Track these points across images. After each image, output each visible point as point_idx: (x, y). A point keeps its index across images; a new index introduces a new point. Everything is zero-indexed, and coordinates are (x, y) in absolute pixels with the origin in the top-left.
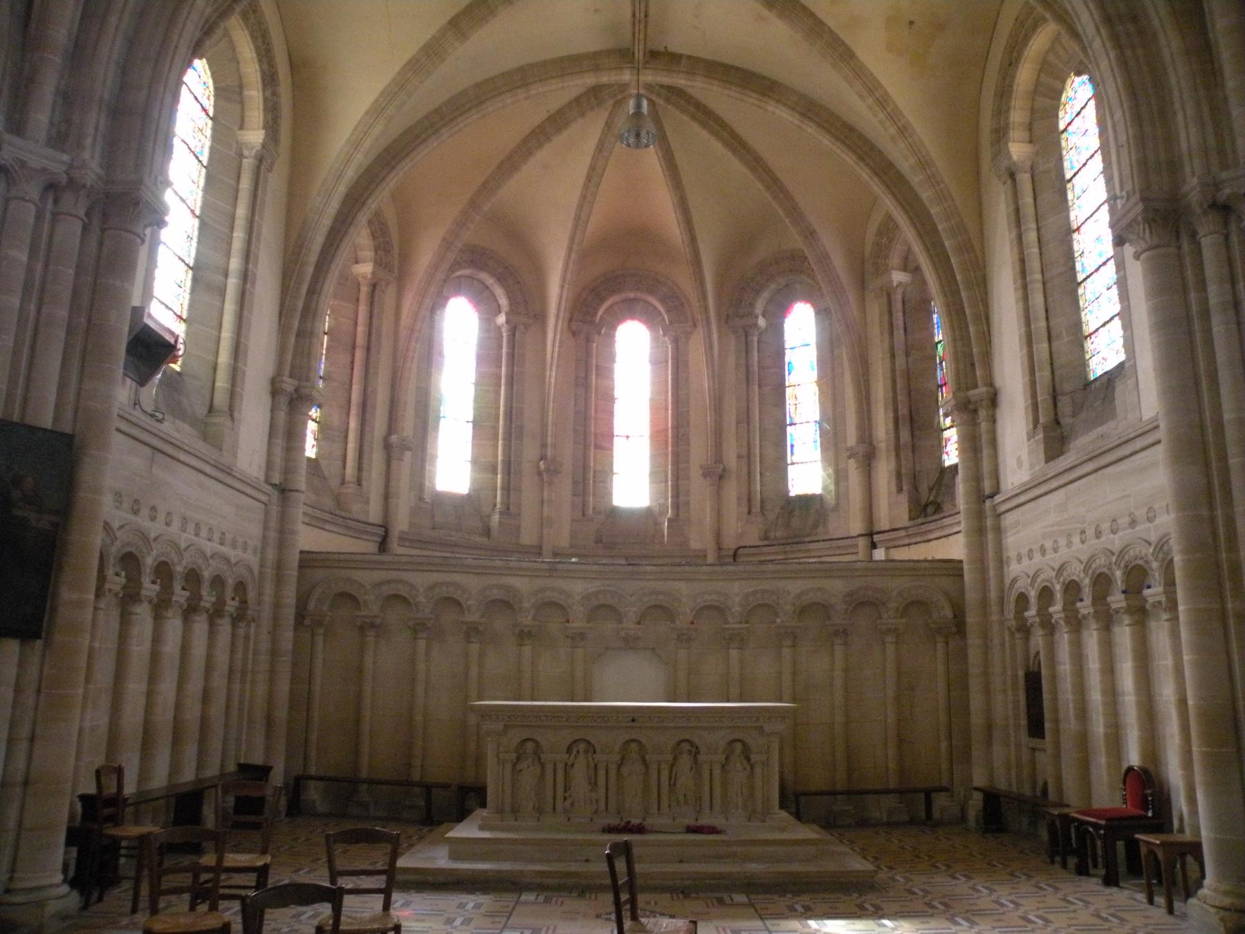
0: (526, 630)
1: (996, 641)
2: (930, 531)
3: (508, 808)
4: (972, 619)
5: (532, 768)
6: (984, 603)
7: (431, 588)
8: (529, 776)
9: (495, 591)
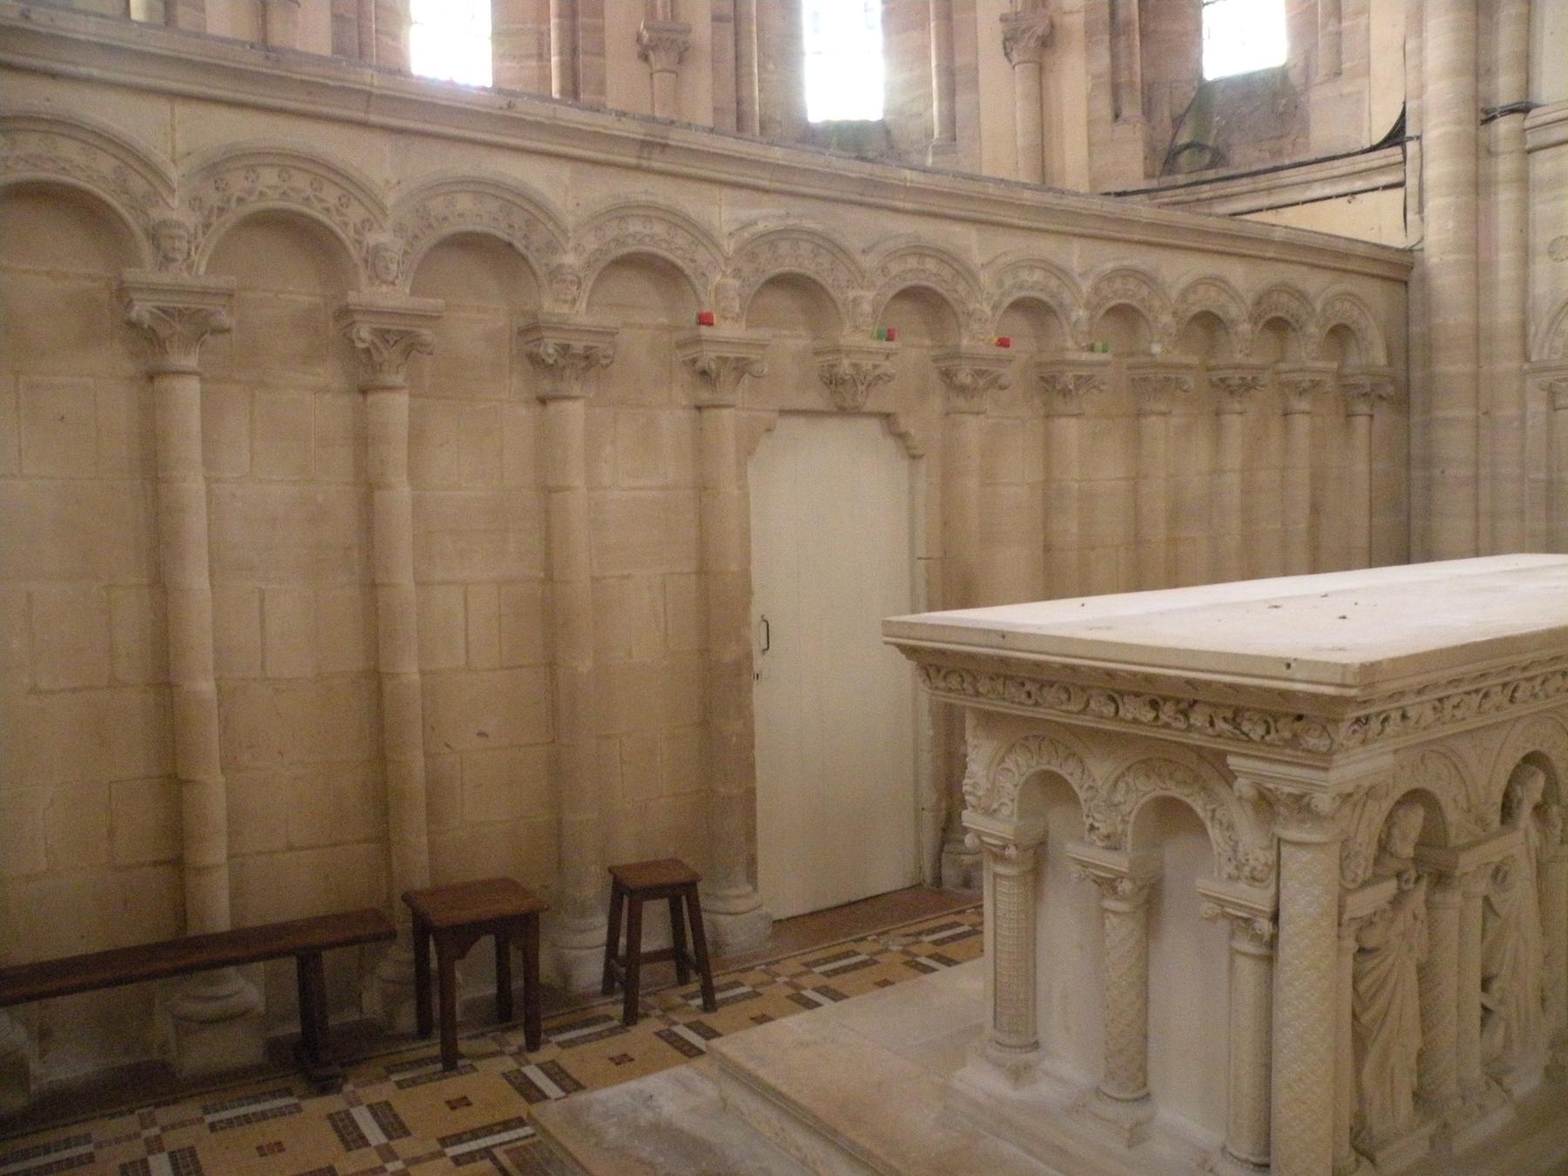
0: (579, 346)
2: (1308, 183)
4: (1452, 367)
6: (1480, 337)
7: (213, 169)
9: (464, 203)
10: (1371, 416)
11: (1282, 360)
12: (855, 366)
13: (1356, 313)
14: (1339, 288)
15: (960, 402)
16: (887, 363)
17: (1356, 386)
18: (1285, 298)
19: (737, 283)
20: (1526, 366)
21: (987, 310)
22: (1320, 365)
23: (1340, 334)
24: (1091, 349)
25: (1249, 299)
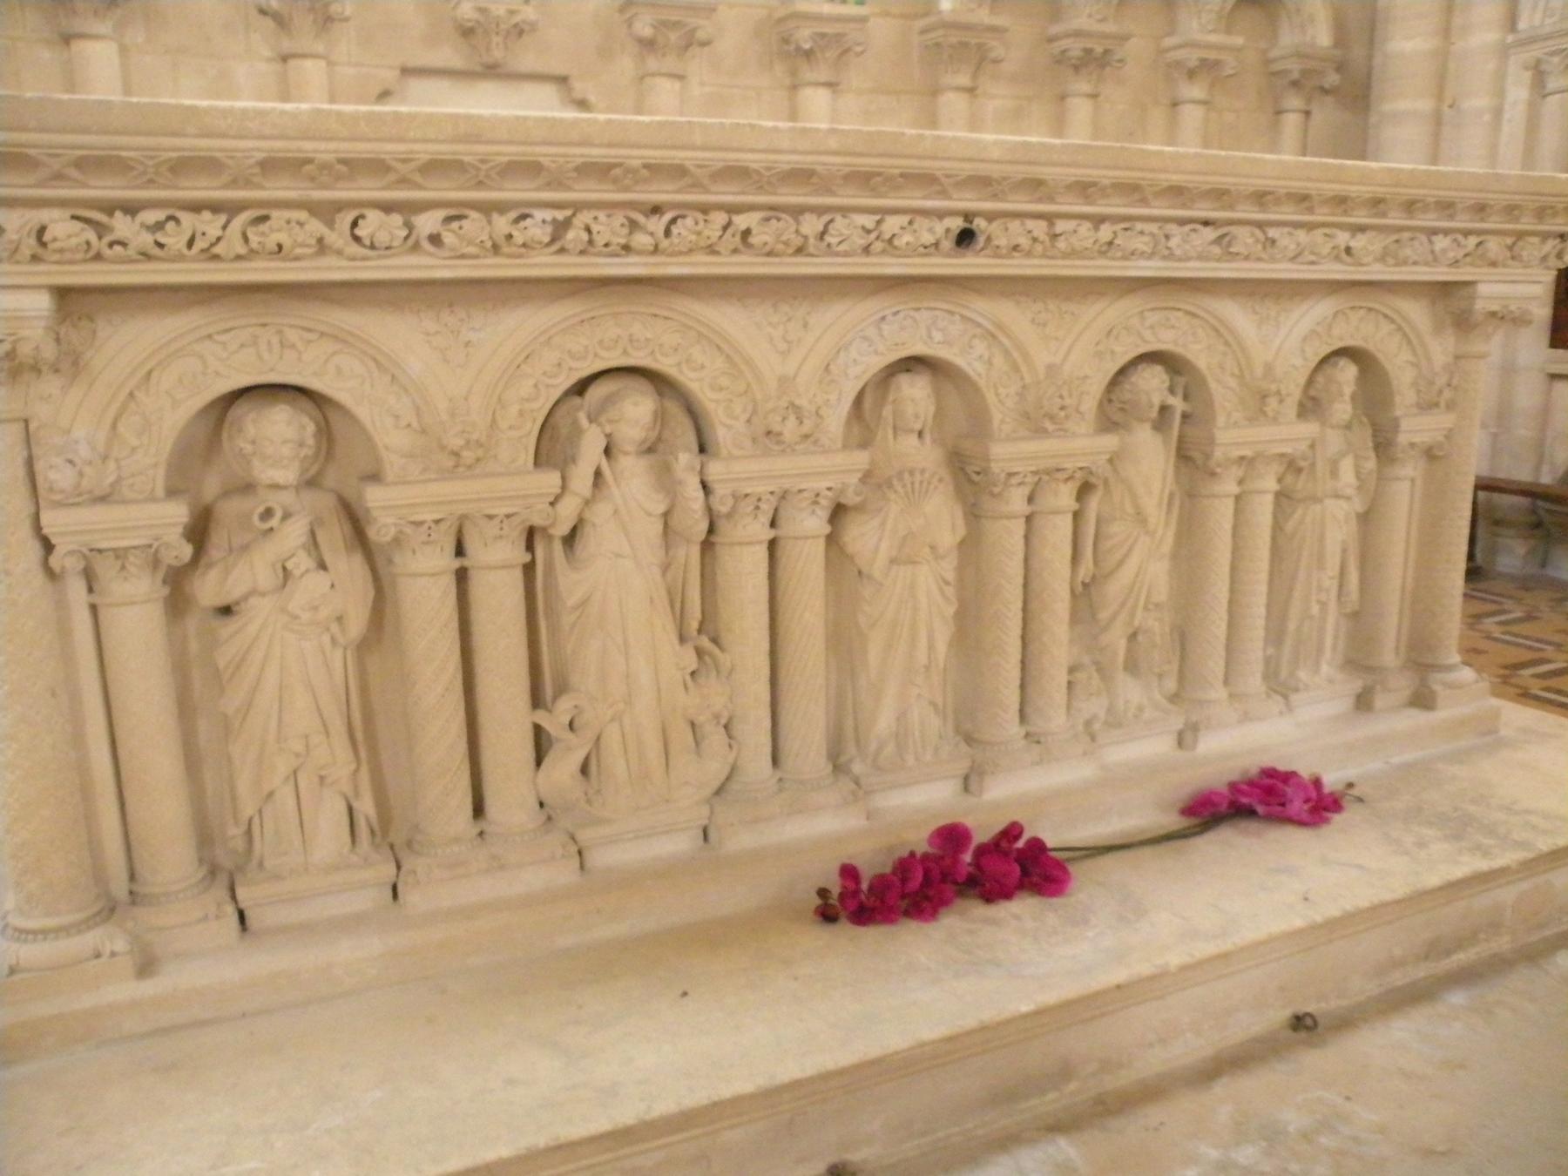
1: (1479, 102)
5: (316, 583)
8: (291, 623)
10: (1307, 113)
11: (1171, 34)
15: (652, 63)
20: (1510, 38)
22: (1213, 38)
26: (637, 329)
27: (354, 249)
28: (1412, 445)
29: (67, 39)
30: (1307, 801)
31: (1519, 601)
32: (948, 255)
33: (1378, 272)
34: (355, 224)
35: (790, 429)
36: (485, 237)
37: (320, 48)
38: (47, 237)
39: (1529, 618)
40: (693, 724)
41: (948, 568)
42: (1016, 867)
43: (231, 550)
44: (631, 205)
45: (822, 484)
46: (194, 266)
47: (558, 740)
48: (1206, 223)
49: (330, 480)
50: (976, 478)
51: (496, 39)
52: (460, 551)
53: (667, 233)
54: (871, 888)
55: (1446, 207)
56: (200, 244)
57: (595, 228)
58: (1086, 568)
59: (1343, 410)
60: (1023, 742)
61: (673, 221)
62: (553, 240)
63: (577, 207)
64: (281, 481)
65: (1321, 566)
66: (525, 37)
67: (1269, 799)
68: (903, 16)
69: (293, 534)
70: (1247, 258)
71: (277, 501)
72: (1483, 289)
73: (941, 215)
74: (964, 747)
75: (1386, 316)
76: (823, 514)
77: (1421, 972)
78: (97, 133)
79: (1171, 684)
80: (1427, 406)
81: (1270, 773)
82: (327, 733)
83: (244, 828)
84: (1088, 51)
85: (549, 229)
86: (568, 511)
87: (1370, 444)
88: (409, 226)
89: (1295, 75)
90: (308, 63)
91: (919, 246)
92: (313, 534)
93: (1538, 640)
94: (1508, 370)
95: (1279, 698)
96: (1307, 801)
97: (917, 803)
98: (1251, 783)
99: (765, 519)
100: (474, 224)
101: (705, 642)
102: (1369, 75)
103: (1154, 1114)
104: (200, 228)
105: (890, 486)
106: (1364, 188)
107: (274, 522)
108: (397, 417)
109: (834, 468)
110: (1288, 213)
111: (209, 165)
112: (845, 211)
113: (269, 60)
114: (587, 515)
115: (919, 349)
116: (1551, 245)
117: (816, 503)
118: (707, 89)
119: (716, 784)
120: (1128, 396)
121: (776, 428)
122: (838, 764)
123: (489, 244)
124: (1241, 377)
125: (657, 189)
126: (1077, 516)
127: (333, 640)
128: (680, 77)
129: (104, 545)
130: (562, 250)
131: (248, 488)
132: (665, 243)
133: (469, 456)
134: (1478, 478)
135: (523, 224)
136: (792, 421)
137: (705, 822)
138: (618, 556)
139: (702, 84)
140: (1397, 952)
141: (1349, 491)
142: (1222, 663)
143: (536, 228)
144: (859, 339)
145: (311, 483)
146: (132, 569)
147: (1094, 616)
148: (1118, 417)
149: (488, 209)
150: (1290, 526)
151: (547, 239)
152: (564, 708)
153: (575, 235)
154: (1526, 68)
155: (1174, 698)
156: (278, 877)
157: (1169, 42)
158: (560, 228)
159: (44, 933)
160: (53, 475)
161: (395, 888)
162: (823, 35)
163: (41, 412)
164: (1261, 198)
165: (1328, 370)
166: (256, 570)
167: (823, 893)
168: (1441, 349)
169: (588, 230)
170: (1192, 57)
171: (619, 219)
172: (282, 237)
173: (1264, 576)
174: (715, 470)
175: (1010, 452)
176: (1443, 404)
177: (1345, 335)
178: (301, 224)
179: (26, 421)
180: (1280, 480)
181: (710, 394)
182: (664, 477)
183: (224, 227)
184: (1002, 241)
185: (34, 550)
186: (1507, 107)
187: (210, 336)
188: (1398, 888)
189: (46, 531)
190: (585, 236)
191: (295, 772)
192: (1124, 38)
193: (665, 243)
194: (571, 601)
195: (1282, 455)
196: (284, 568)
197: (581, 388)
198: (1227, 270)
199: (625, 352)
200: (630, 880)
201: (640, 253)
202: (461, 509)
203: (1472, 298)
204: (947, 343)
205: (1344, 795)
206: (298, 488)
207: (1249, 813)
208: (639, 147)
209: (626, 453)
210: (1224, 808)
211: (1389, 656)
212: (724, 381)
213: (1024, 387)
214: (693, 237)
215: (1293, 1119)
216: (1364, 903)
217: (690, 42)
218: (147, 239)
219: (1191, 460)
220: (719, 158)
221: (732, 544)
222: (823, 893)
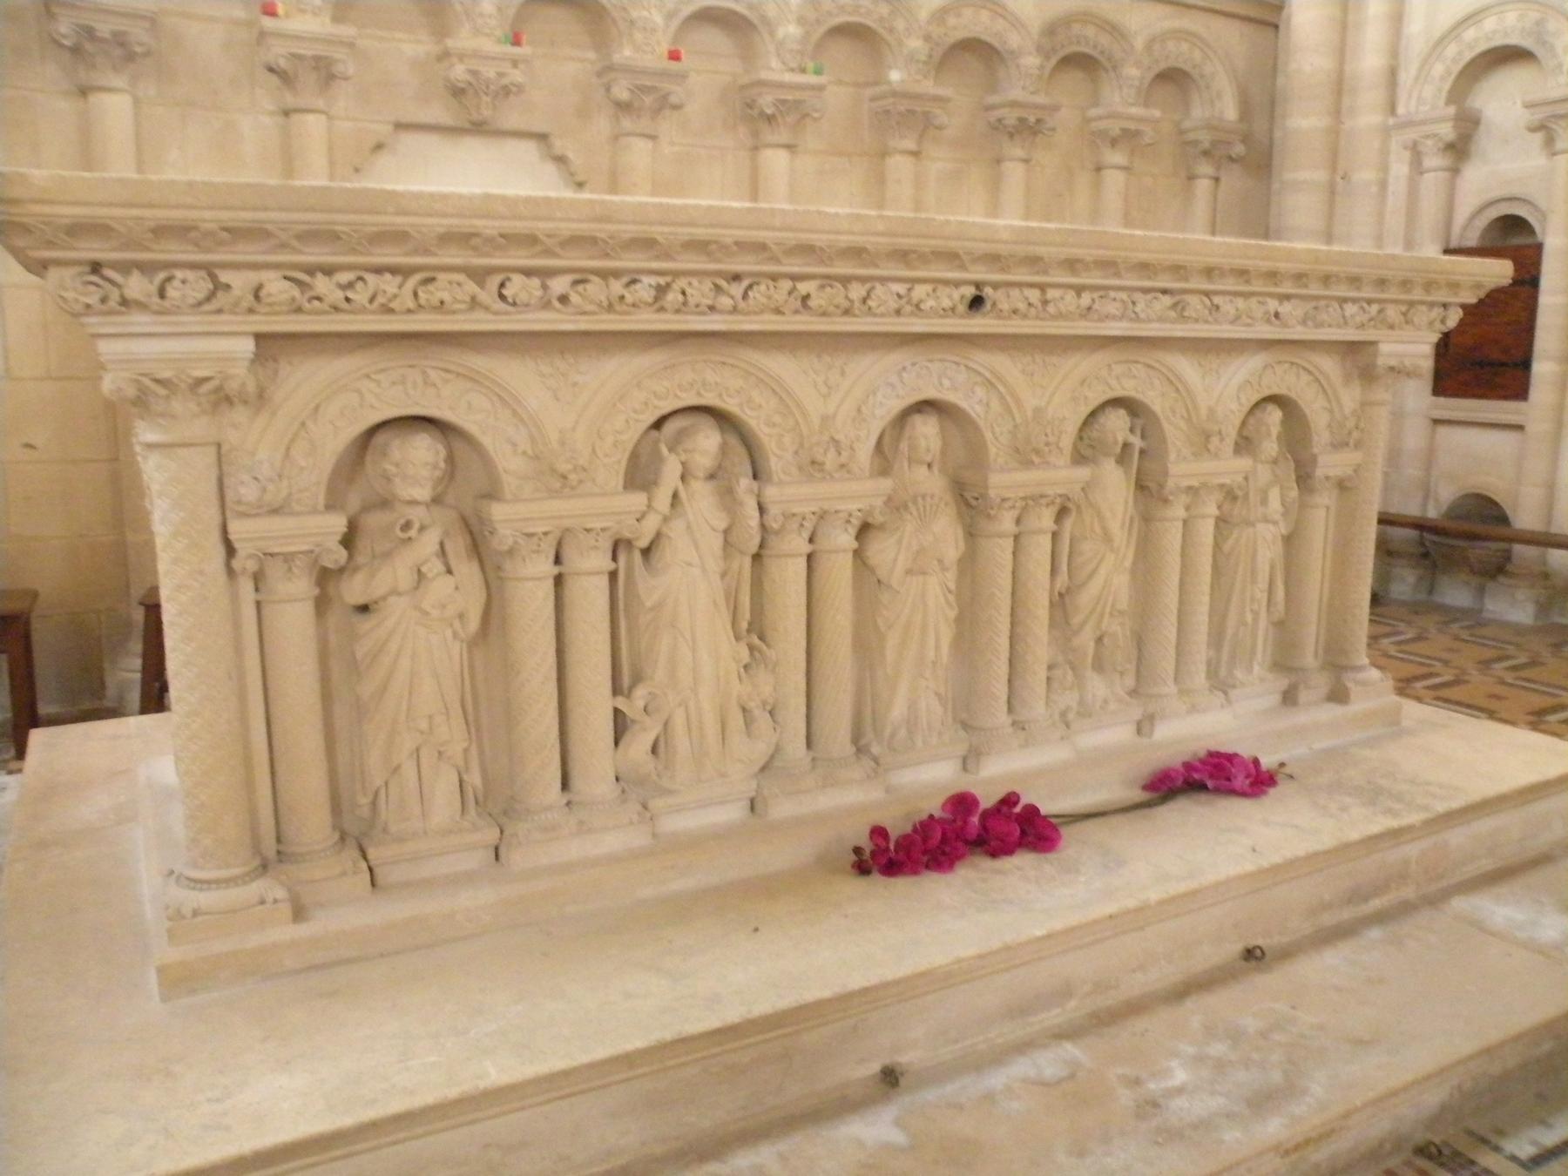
1: (1366, 175)
3: (313, 825)
4: (1304, 121)
5: (441, 587)
6: (1340, 86)
8: (422, 619)
10: (1217, 179)
11: (1096, 104)
12: (474, 73)
13: (1197, 55)
14: (1168, 24)
15: (627, 124)
16: (516, 72)
17: (1195, 143)
18: (1090, 31)
19: (1230, 112)
20: (1391, 121)
21: (658, 19)
22: (1134, 110)
23: (1173, 79)
24: (803, 71)
25: (1035, 27)
26: (710, 376)
27: (501, 306)
28: (1327, 478)
29: (84, 92)
30: (1247, 777)
31: (1409, 623)
32: (962, 317)
33: (1298, 333)
34: (502, 285)
35: (830, 460)
36: (603, 298)
37: (320, 103)
38: (263, 293)
39: (1419, 638)
40: (744, 710)
41: (951, 577)
42: (1014, 829)
43: (374, 557)
44: (719, 274)
45: (853, 506)
46: (371, 317)
47: (633, 721)
48: (1165, 292)
49: (450, 499)
50: (974, 503)
51: (485, 98)
52: (558, 560)
53: (745, 296)
54: (897, 844)
55: (1355, 281)
56: (380, 300)
57: (689, 291)
58: (1062, 579)
59: (1271, 447)
60: (1010, 730)
61: (750, 287)
62: (656, 299)
63: (677, 274)
64: (419, 498)
65: (1254, 581)
66: (512, 97)
67: (1217, 776)
68: (857, 85)
69: (428, 543)
70: (1197, 321)
71: (417, 515)
72: (1384, 348)
73: (957, 284)
74: (962, 733)
75: (1305, 369)
76: (853, 531)
77: (1346, 914)
78: (322, 211)
79: (1130, 681)
80: (1339, 445)
81: (1214, 755)
82: (448, 714)
83: (371, 798)
84: (1022, 120)
85: (653, 292)
86: (651, 525)
87: (1294, 477)
88: (545, 287)
89: (1207, 145)
90: (310, 118)
91: (939, 309)
92: (442, 545)
93: (1429, 657)
94: (1398, 416)
95: (1220, 694)
96: (1247, 777)
97: (926, 781)
98: (1203, 762)
99: (806, 535)
100: (595, 288)
101: (756, 641)
102: (1271, 147)
103: (1140, 1024)
104: (383, 287)
105: (906, 507)
106: (1290, 265)
107: (413, 533)
108: (514, 445)
109: (862, 493)
110: (1230, 284)
111: (398, 237)
112: (883, 280)
113: (272, 113)
114: (665, 530)
115: (930, 393)
116: (1437, 312)
117: (848, 522)
118: (676, 149)
119: (762, 763)
120: (1095, 434)
121: (819, 458)
122: (861, 750)
123: (605, 304)
124: (1189, 420)
125: (736, 262)
126: (1055, 535)
127: (455, 635)
128: (653, 137)
129: (276, 550)
130: (662, 309)
131: (385, 503)
132: (742, 305)
133: (573, 477)
134: (1380, 513)
135: (633, 287)
136: (832, 454)
137: (753, 794)
138: (690, 564)
139: (672, 144)
140: (1327, 897)
141: (1277, 517)
142: (1173, 662)
143: (644, 291)
144: (883, 384)
145: (437, 500)
146: (295, 570)
147: (1067, 623)
148: (1087, 452)
149: (605, 275)
150: (1226, 547)
151: (650, 300)
152: (640, 693)
153: (673, 297)
154: (1405, 148)
155: (1134, 693)
156: (401, 840)
157: (1093, 112)
158: (661, 290)
159: (218, 882)
160: (243, 491)
161: (497, 849)
162: (784, 102)
163: (232, 437)
164: (1209, 272)
165: (1258, 413)
166: (398, 572)
167: (857, 851)
168: (1350, 397)
169: (684, 293)
170: (1115, 127)
171: (707, 285)
172: (446, 296)
173: (1206, 588)
174: (771, 492)
175: (1005, 481)
176: (1352, 442)
177: (1278, 382)
178: (459, 284)
179: (219, 446)
180: (1219, 507)
181: (766, 430)
182: (727, 497)
183: (400, 287)
184: (1005, 306)
185: (219, 552)
186: (1391, 180)
187: (368, 376)
188: (1326, 841)
189: (232, 537)
190: (680, 298)
191: (418, 750)
192: (1055, 108)
193: (742, 305)
194: (648, 604)
195: (1222, 486)
196: (419, 571)
197: (658, 424)
198: (1179, 331)
199: (699, 394)
200: (694, 842)
201: (721, 312)
202: (567, 523)
203: (1375, 355)
204: (954, 389)
205: (1277, 772)
206: (427, 505)
207: (1201, 787)
208: (731, 227)
209: (696, 478)
210: (1179, 782)
211: (1309, 658)
212: (777, 419)
213: (1016, 426)
214: (764, 300)
215: (1251, 1024)
216: (1301, 853)
217: (664, 104)
218: (340, 294)
219: (1149, 489)
220: (790, 238)
221: (778, 556)
222: (857, 851)
